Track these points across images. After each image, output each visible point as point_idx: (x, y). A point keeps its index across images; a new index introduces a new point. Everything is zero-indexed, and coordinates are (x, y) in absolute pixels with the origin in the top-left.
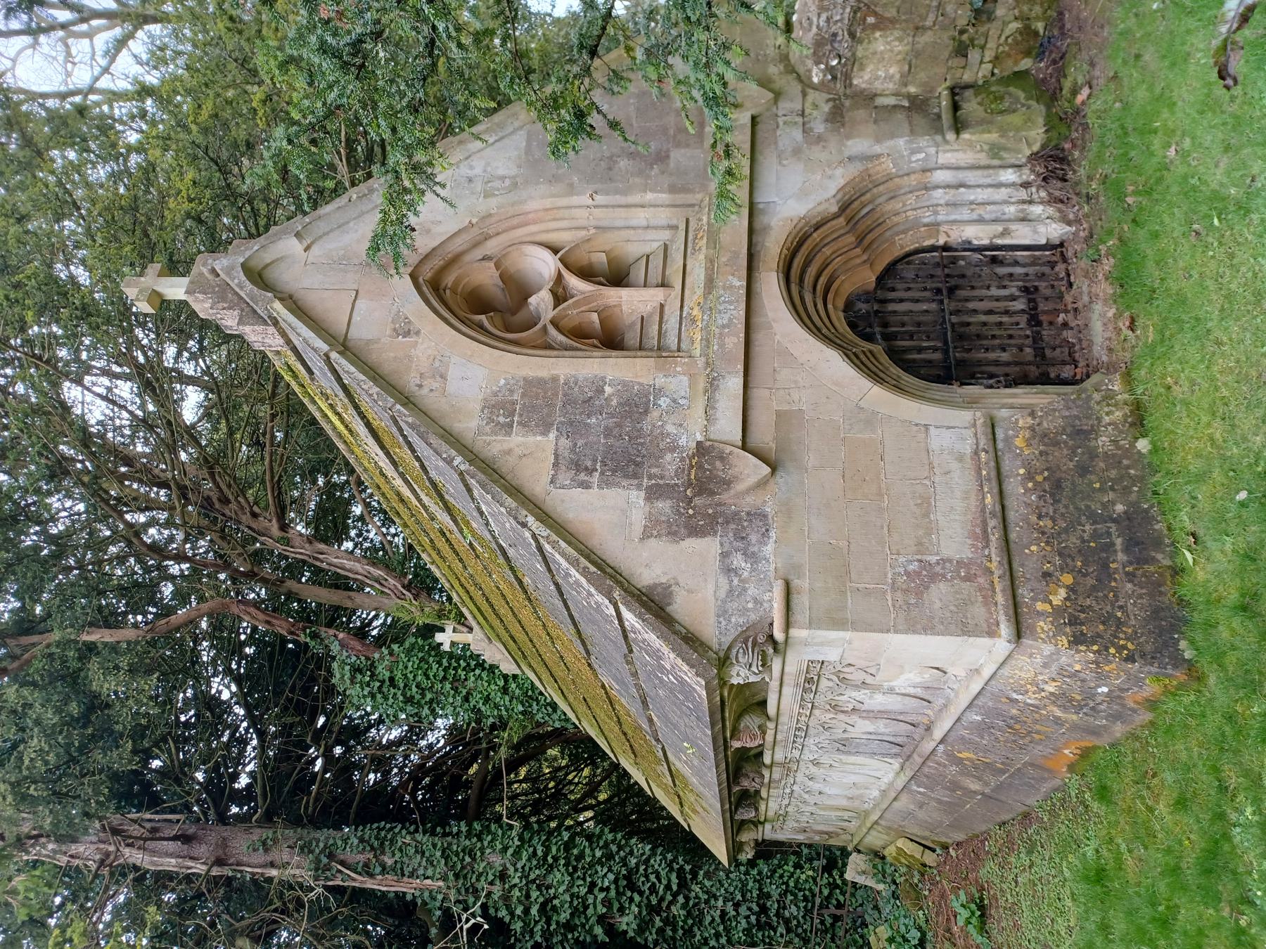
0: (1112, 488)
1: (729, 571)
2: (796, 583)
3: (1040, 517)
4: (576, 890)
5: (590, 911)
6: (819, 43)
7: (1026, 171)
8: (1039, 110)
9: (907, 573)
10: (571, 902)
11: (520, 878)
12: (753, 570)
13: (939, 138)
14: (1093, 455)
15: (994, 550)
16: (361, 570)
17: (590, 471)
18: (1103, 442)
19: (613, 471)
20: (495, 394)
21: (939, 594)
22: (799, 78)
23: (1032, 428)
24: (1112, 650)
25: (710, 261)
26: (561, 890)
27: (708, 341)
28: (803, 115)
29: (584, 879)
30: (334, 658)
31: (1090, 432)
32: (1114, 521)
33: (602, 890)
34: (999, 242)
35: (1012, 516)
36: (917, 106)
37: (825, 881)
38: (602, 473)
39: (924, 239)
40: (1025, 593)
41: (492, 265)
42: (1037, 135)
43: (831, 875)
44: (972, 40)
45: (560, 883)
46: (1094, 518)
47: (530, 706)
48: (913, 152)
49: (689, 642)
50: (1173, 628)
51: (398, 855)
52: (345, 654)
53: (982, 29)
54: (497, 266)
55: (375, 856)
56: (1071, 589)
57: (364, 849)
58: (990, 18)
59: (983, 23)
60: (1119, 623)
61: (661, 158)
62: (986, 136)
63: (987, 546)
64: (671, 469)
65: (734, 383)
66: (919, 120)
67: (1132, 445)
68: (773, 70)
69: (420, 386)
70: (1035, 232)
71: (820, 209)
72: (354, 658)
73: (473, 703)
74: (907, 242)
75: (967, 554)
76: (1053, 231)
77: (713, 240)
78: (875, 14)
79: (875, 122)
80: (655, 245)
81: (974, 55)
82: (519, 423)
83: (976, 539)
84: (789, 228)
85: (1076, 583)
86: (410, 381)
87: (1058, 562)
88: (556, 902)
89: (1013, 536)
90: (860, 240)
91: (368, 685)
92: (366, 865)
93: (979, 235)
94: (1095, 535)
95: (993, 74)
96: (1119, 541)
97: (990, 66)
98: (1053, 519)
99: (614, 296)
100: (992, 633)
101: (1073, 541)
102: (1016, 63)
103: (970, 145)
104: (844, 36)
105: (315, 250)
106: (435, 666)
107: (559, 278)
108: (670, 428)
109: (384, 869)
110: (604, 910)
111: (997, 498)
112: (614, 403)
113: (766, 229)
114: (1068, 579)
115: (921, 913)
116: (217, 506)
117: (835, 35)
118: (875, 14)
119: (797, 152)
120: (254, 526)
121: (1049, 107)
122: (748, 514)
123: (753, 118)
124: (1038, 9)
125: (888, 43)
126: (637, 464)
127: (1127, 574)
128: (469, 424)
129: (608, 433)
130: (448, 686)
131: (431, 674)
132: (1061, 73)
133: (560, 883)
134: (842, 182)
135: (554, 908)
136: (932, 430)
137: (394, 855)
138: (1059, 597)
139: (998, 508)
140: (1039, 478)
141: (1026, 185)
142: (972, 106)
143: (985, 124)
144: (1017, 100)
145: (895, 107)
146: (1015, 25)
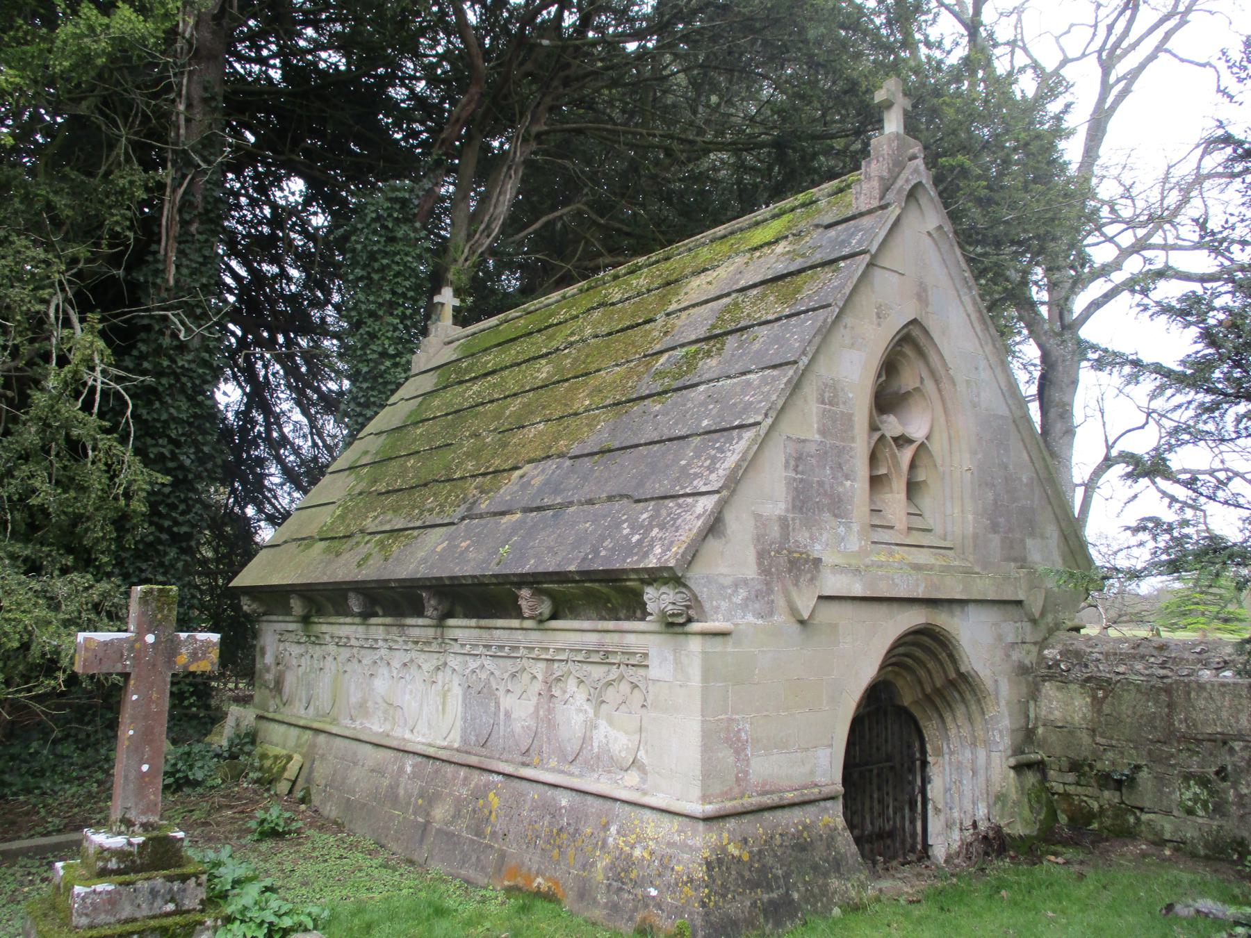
1: (736, 585)
2: (730, 640)
3: (781, 835)
4: (173, 426)
5: (149, 441)
6: (1078, 654)
7: (986, 824)
10: (158, 420)
11: (182, 367)
13: (1009, 752)
14: (826, 875)
16: (498, 211)
18: (834, 883)
19: (796, 489)
20: (842, 390)
21: (726, 756)
22: (1045, 639)
23: (836, 829)
25: (931, 568)
26: (172, 410)
28: (1023, 643)
29: (183, 435)
32: (787, 892)
34: (930, 807)
35: (779, 813)
36: (1028, 735)
38: (795, 480)
40: (731, 824)
41: (918, 385)
43: (192, 694)
44: (1084, 774)
45: (178, 409)
46: (787, 876)
47: (365, 380)
48: (1000, 732)
49: (693, 554)
51: (202, 238)
52: (421, 193)
53: (1093, 782)
54: (917, 390)
55: (200, 214)
56: (740, 860)
57: (208, 203)
58: (1102, 787)
59: (1097, 782)
60: (724, 896)
62: (1013, 790)
63: (759, 795)
65: (858, 590)
66: (1021, 735)
67: (836, 904)
68: (1050, 618)
69: (845, 327)
70: (938, 835)
71: (965, 659)
72: (416, 202)
73: (370, 321)
74: (930, 730)
75: (753, 778)
76: (939, 851)
77: (946, 569)
78: (1105, 697)
79: (1019, 701)
80: (931, 522)
81: (1071, 777)
83: (763, 786)
84: (954, 632)
85: (744, 863)
86: (848, 320)
87: (755, 849)
88: (157, 405)
89: (766, 814)
90: (938, 692)
91: (390, 215)
92: (191, 204)
93: (935, 790)
94: (776, 878)
97: (1061, 791)
98: (781, 846)
99: (899, 485)
100: (705, 799)
101: (770, 861)
102: (1064, 811)
103: (1005, 778)
105: (928, 240)
106: (407, 284)
107: (910, 441)
108: (825, 536)
109: (185, 224)
110: (152, 456)
112: (841, 490)
113: (952, 614)
114: (746, 857)
115: (220, 781)
116: (562, 74)
118: (1105, 697)
119: (1000, 638)
122: (773, 601)
123: (1019, 603)
124: (1108, 822)
125: (1080, 709)
127: (755, 902)
128: (823, 370)
129: (821, 484)
130: (388, 297)
131: (399, 280)
133: (178, 409)
135: (150, 403)
136: (828, 751)
138: (733, 850)
139: (786, 802)
140: (805, 834)
141: (975, 825)
142: (1031, 778)
143: (1022, 789)
144: (1038, 814)
146: (1095, 806)
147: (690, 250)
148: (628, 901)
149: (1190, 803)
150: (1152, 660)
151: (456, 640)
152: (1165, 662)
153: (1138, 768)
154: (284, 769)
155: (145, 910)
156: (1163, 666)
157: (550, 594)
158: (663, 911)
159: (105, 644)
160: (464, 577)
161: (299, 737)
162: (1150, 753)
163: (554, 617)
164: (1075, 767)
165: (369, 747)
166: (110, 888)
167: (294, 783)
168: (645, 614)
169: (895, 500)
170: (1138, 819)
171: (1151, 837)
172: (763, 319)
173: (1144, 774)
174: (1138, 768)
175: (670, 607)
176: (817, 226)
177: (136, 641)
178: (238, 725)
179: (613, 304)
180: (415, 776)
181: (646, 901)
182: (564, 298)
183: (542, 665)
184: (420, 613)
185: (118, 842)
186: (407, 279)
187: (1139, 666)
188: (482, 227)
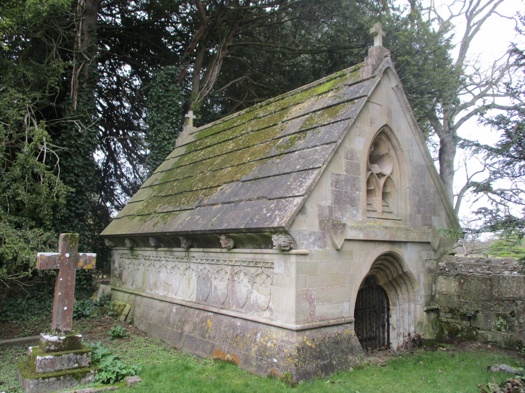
0: (339, 360)
1: (310, 234)
2: (308, 257)
3: (328, 338)
4: (76, 168)
5: (66, 174)
6: (453, 264)
7: (414, 334)
8: (433, 337)
9: (311, 294)
10: (70, 166)
12: (311, 242)
13: (424, 305)
14: (347, 354)
15: (318, 323)
16: (212, 78)
17: (336, 187)
18: (350, 357)
19: (336, 195)
21: (306, 305)
22: (440, 258)
24: (297, 360)
25: (392, 228)
26: (76, 162)
27: (371, 227)
29: (80, 172)
30: (178, 66)
31: (352, 353)
32: (331, 361)
33: (76, 179)
34: (391, 327)
35: (328, 329)
37: (82, 277)
38: (335, 191)
39: (392, 302)
40: (308, 333)
41: (387, 152)
42: (428, 337)
43: (84, 280)
45: (78, 161)
46: (330, 354)
48: (420, 296)
49: (292, 221)
50: (306, 378)
52: (180, 71)
53: (459, 317)
54: (387, 154)
56: (311, 348)
57: (90, 75)
58: (462, 319)
59: (461, 317)
61: (419, 212)
62: (425, 320)
64: (337, 215)
65: (361, 237)
66: (428, 299)
67: (351, 366)
70: (394, 339)
72: (178, 75)
73: (158, 125)
74: (391, 295)
75: (317, 314)
76: (394, 345)
77: (398, 229)
78: (464, 282)
81: (450, 315)
82: (348, 162)
83: (321, 317)
84: (401, 255)
85: (313, 349)
86: (358, 124)
87: (318, 343)
88: (70, 159)
90: (394, 279)
91: (167, 80)
92: (83, 76)
93: (393, 320)
94: (326, 355)
95: (442, 322)
96: (325, 362)
97: (445, 321)
98: (328, 342)
99: (379, 194)
100: (297, 322)
101: (324, 348)
102: (447, 329)
103: (422, 316)
104: (456, 272)
105: (392, 91)
106: (174, 109)
107: (384, 175)
108: (348, 214)
109: (81, 84)
110: (67, 181)
111: (333, 324)
114: (314, 346)
116: (239, 21)
117: (456, 269)
118: (464, 282)
119: (420, 257)
120: (230, 35)
121: (435, 340)
123: (429, 243)
126: (338, 203)
129: (346, 193)
130: (166, 115)
131: (170, 107)
132: (447, 342)
133: (78, 161)
134: (413, 273)
136: (348, 303)
137: (87, 88)
138: (308, 343)
140: (338, 338)
142: (433, 315)
143: (429, 320)
144: (436, 330)
145: (432, 290)
146: (460, 327)
147: (292, 95)
148: (265, 364)
149: (499, 326)
150: (484, 267)
151: (194, 257)
152: (489, 268)
153: (477, 312)
154: (123, 310)
155: (66, 366)
156: (488, 269)
157: (233, 238)
158: (279, 368)
159: (49, 257)
160: (197, 231)
161: (129, 297)
162: (483, 305)
163: (235, 247)
164: (451, 311)
165: (158, 302)
166: (52, 357)
167: (127, 316)
168: (273, 246)
169: (377, 200)
170: (477, 333)
171: (483, 340)
172: (323, 124)
173: (480, 314)
174: (477, 312)
175: (283, 243)
176: (346, 85)
177: (61, 256)
178: (103, 292)
179: (260, 118)
180: (177, 313)
181: (272, 364)
182: (239, 115)
183: (230, 267)
184: (179, 246)
185: (55, 338)
186: (174, 107)
187: (478, 269)
188: (205, 85)
